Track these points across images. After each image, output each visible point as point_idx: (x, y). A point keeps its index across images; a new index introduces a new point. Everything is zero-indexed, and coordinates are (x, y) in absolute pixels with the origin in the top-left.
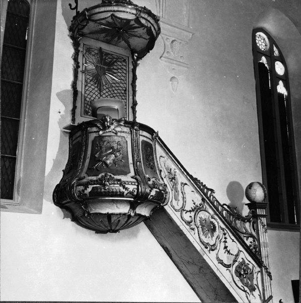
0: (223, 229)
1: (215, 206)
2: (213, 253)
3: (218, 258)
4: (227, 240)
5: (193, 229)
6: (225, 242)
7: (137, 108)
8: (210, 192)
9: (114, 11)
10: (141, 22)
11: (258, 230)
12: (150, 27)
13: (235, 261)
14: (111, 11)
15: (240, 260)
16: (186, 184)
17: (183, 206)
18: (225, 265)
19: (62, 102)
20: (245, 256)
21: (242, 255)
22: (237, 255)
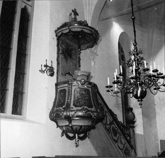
0: (120, 133)
1: (118, 122)
2: (116, 144)
3: (118, 146)
4: (121, 140)
5: (110, 133)
6: (121, 139)
7: (81, 61)
8: (115, 116)
9: (62, 31)
10: (82, 134)
11: (152, 41)
12: (82, 30)
13: (124, 147)
14: (61, 31)
15: (125, 147)
16: (107, 112)
17: (106, 122)
18: (121, 149)
19: (53, 121)
20: (127, 145)
21: (126, 145)
22: (124, 145)
